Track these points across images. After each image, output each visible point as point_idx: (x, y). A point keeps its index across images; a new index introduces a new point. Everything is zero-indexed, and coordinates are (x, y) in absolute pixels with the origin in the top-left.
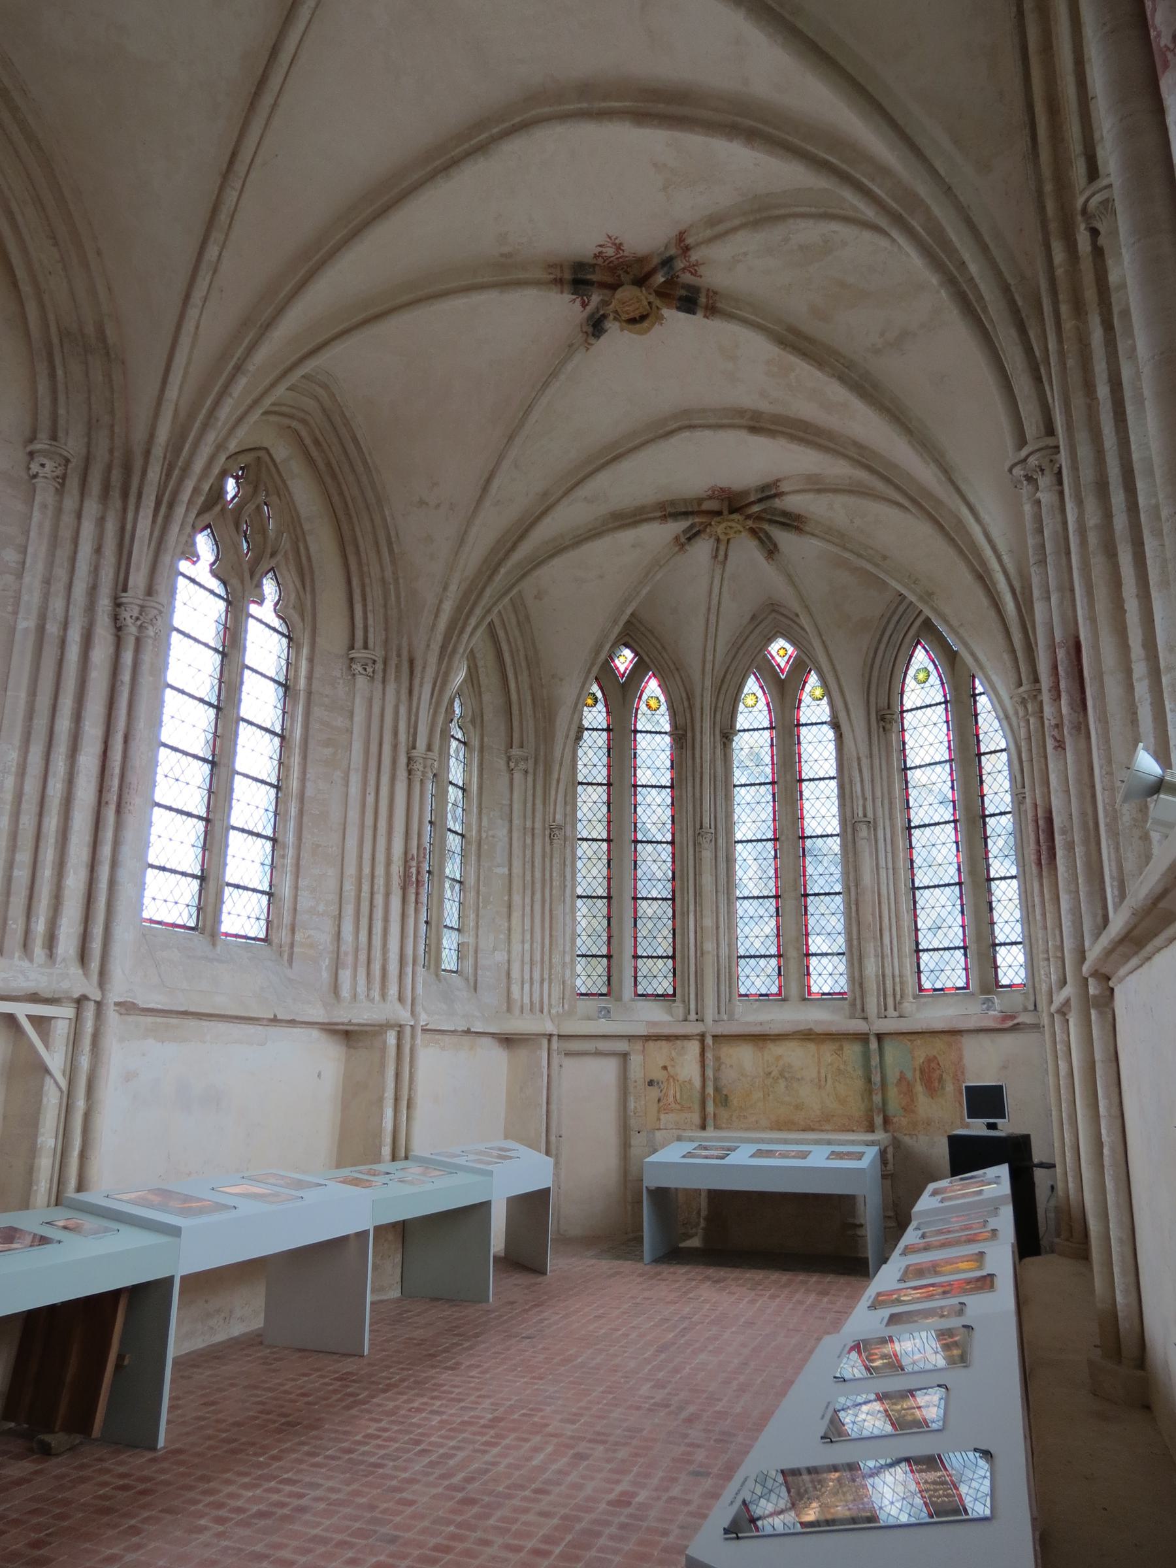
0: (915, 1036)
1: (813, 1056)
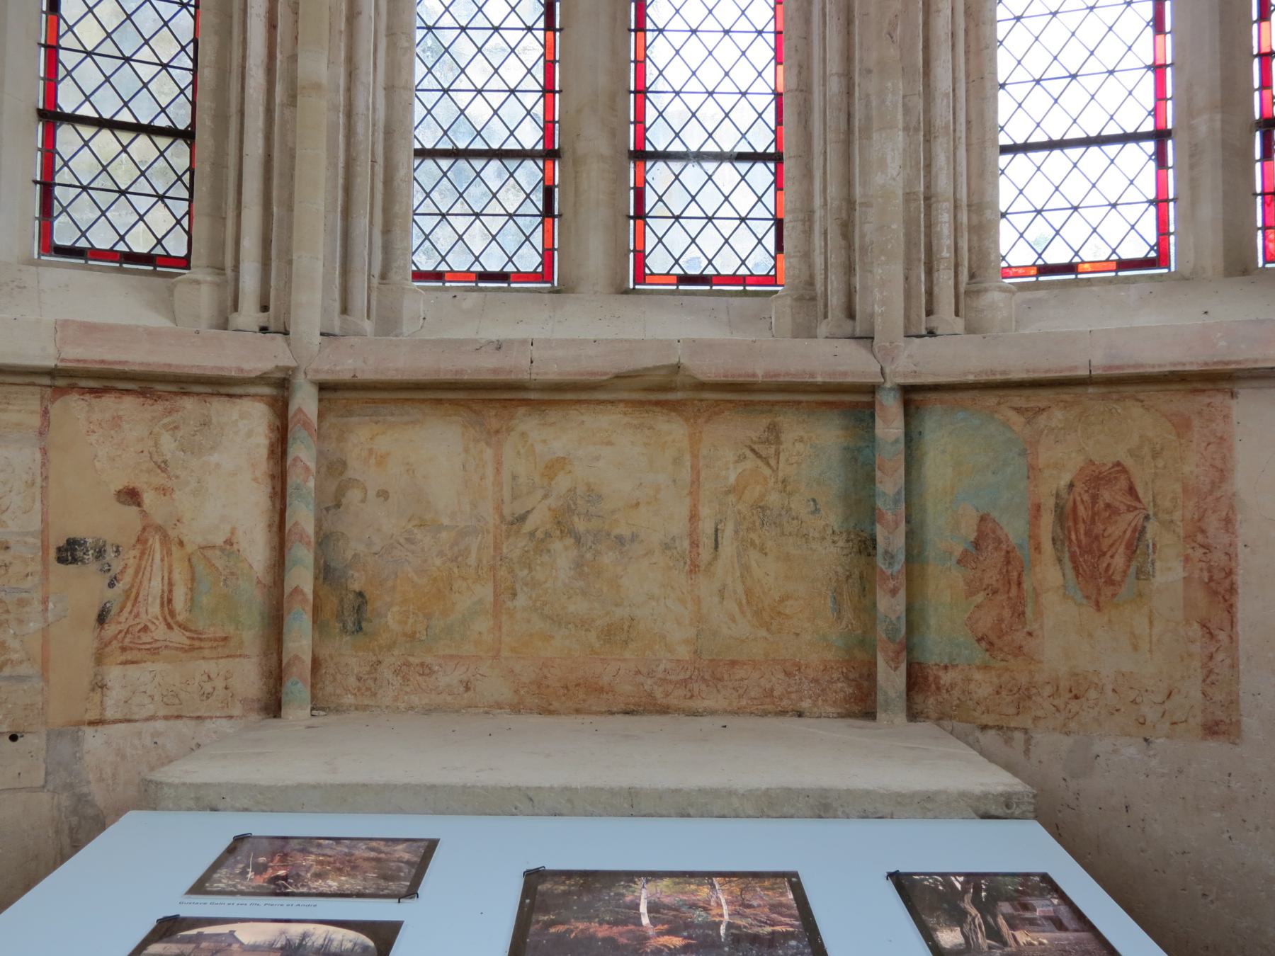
0: (1042, 398)
1: (677, 461)
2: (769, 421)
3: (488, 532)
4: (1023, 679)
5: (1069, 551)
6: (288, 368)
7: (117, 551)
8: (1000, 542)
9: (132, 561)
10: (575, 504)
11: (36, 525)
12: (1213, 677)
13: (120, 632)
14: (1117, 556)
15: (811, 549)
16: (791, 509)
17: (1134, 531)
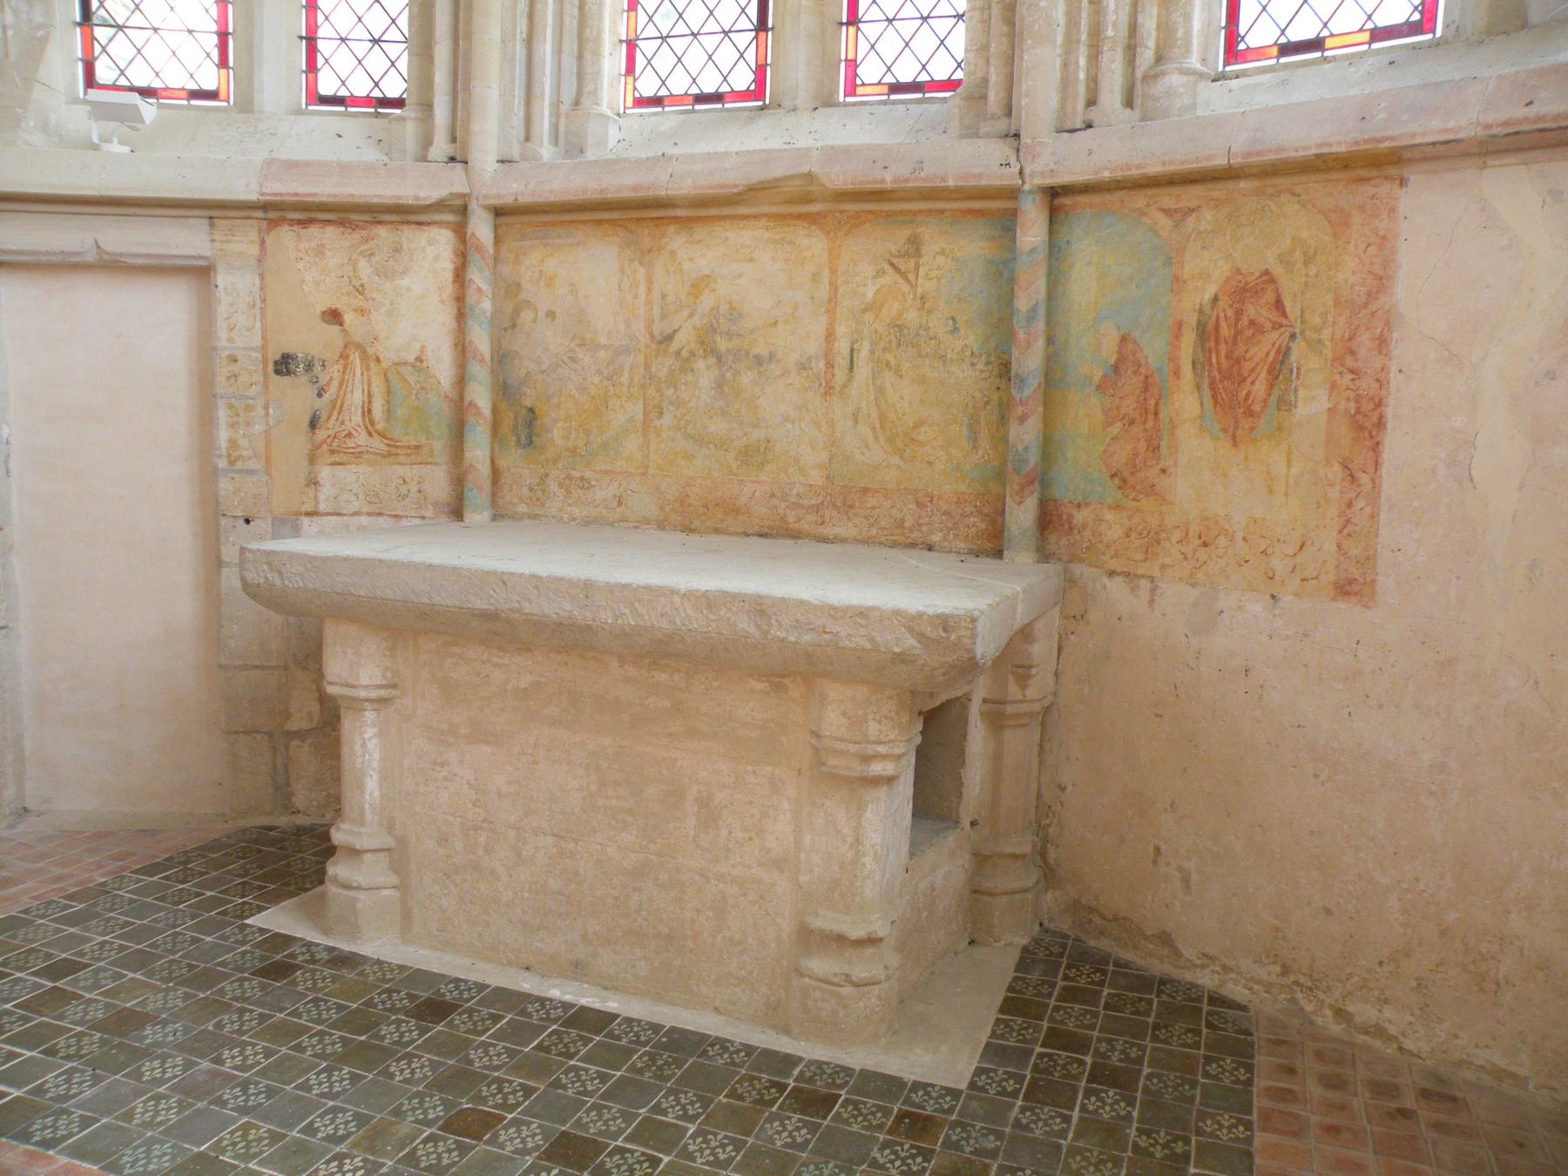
1: (815, 277)
2: (910, 232)
3: (639, 350)
4: (1154, 522)
5: (1209, 376)
6: (463, 196)
7: (323, 365)
8: (1139, 365)
9: (336, 374)
10: (718, 323)
11: (257, 341)
12: (1350, 528)
13: (329, 436)
14: (1258, 383)
15: (948, 371)
16: (929, 328)
17: (1278, 352)
